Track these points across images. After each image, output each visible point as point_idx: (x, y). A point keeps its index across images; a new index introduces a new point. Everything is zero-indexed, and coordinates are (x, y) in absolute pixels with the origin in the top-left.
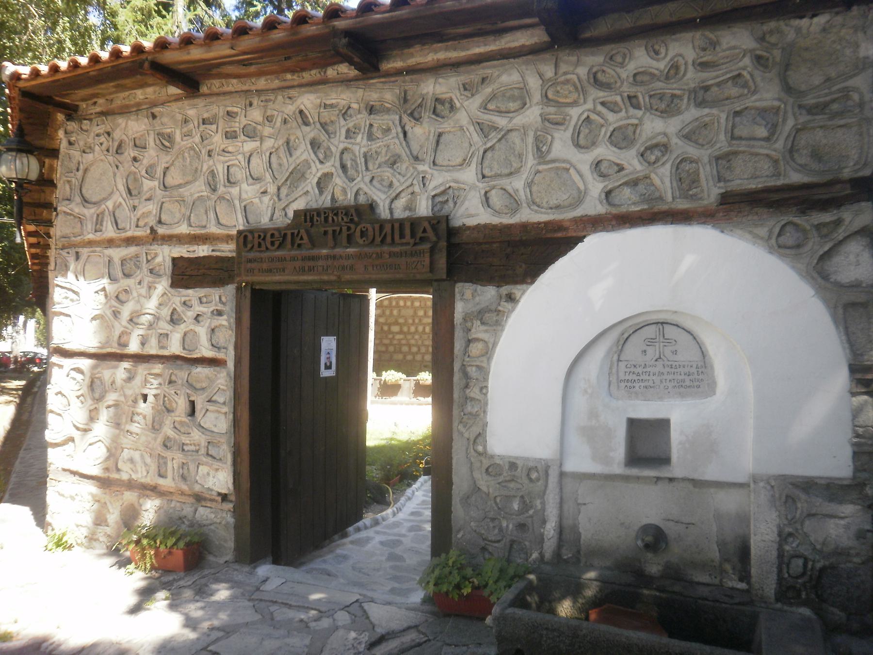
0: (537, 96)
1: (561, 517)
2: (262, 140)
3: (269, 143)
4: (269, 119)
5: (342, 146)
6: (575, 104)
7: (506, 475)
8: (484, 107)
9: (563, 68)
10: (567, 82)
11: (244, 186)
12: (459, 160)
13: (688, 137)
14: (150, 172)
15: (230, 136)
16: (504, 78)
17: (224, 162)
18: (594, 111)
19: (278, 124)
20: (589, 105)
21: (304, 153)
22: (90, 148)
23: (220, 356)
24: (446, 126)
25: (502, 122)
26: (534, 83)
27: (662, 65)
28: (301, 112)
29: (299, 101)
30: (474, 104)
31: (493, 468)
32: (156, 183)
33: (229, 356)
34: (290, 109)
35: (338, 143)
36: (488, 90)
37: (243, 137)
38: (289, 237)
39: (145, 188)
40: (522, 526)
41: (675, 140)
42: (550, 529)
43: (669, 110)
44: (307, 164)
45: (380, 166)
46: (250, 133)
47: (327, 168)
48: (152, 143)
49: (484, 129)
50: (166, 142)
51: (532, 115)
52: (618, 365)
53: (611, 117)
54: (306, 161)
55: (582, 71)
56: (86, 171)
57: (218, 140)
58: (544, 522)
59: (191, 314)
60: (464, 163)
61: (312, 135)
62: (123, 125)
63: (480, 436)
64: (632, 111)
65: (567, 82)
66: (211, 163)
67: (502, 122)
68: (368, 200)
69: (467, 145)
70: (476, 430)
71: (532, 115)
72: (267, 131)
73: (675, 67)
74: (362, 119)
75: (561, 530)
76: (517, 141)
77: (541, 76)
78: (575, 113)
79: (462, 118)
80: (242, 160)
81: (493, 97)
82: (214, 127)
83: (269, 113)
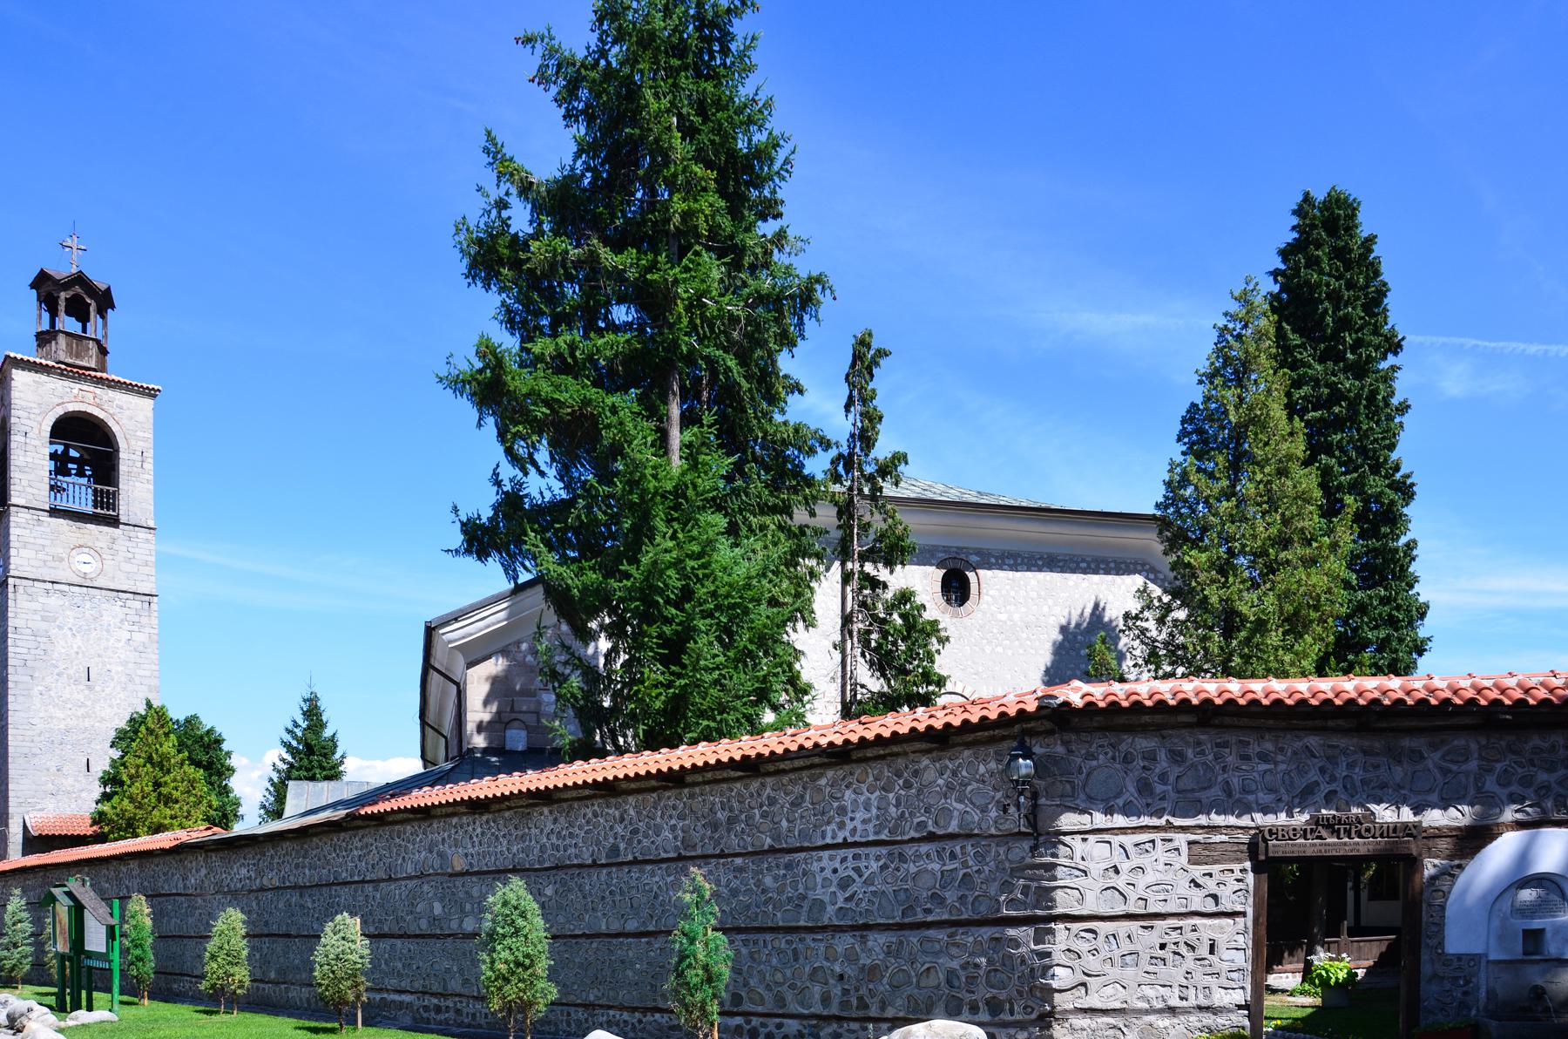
0: (1476, 755)
1: (1487, 984)
2: (1276, 763)
3: (1282, 767)
4: (1281, 750)
5: (1344, 774)
6: (1498, 761)
7: (1456, 964)
8: (1443, 758)
9: (1492, 740)
10: (1493, 748)
11: (1261, 795)
12: (1427, 788)
13: (1560, 783)
14: (1163, 778)
15: (1245, 758)
16: (1456, 742)
17: (1239, 777)
18: (1509, 766)
19: (1289, 754)
20: (1507, 763)
21: (1313, 775)
22: (1093, 755)
23: (1239, 908)
24: (1418, 767)
25: (1454, 767)
26: (1473, 746)
27: (1547, 745)
28: (1307, 747)
29: (1306, 740)
30: (1437, 756)
31: (1447, 960)
32: (1170, 787)
33: (1250, 911)
34: (1298, 744)
35: (1342, 771)
36: (1446, 748)
37: (1257, 760)
38: (1309, 831)
39: (1158, 791)
40: (1465, 993)
41: (1553, 785)
42: (1483, 994)
43: (1551, 769)
44: (1317, 784)
45: (1373, 788)
46: (1263, 757)
47: (1333, 787)
48: (1163, 757)
49: (1445, 772)
50: (1177, 757)
51: (1473, 765)
52: (1488, 947)
53: (1520, 770)
54: (1316, 781)
55: (1503, 743)
56: (1088, 775)
57: (1231, 759)
58: (1479, 988)
59: (837, 865)
60: (1431, 791)
61: (1320, 765)
62: (1130, 740)
63: (1441, 944)
64: (1531, 768)
65: (1493, 748)
66: (1226, 776)
67: (1454, 767)
68: (500, 346)
69: (1432, 779)
70: (1435, 941)
71: (1473, 765)
72: (1280, 758)
73: (1554, 746)
74: (1360, 757)
75: (1487, 992)
76: (1464, 780)
77: (1478, 743)
78: (1499, 766)
79: (1430, 763)
80: (1257, 777)
81: (1447, 753)
82: (1228, 750)
83: (1280, 745)
